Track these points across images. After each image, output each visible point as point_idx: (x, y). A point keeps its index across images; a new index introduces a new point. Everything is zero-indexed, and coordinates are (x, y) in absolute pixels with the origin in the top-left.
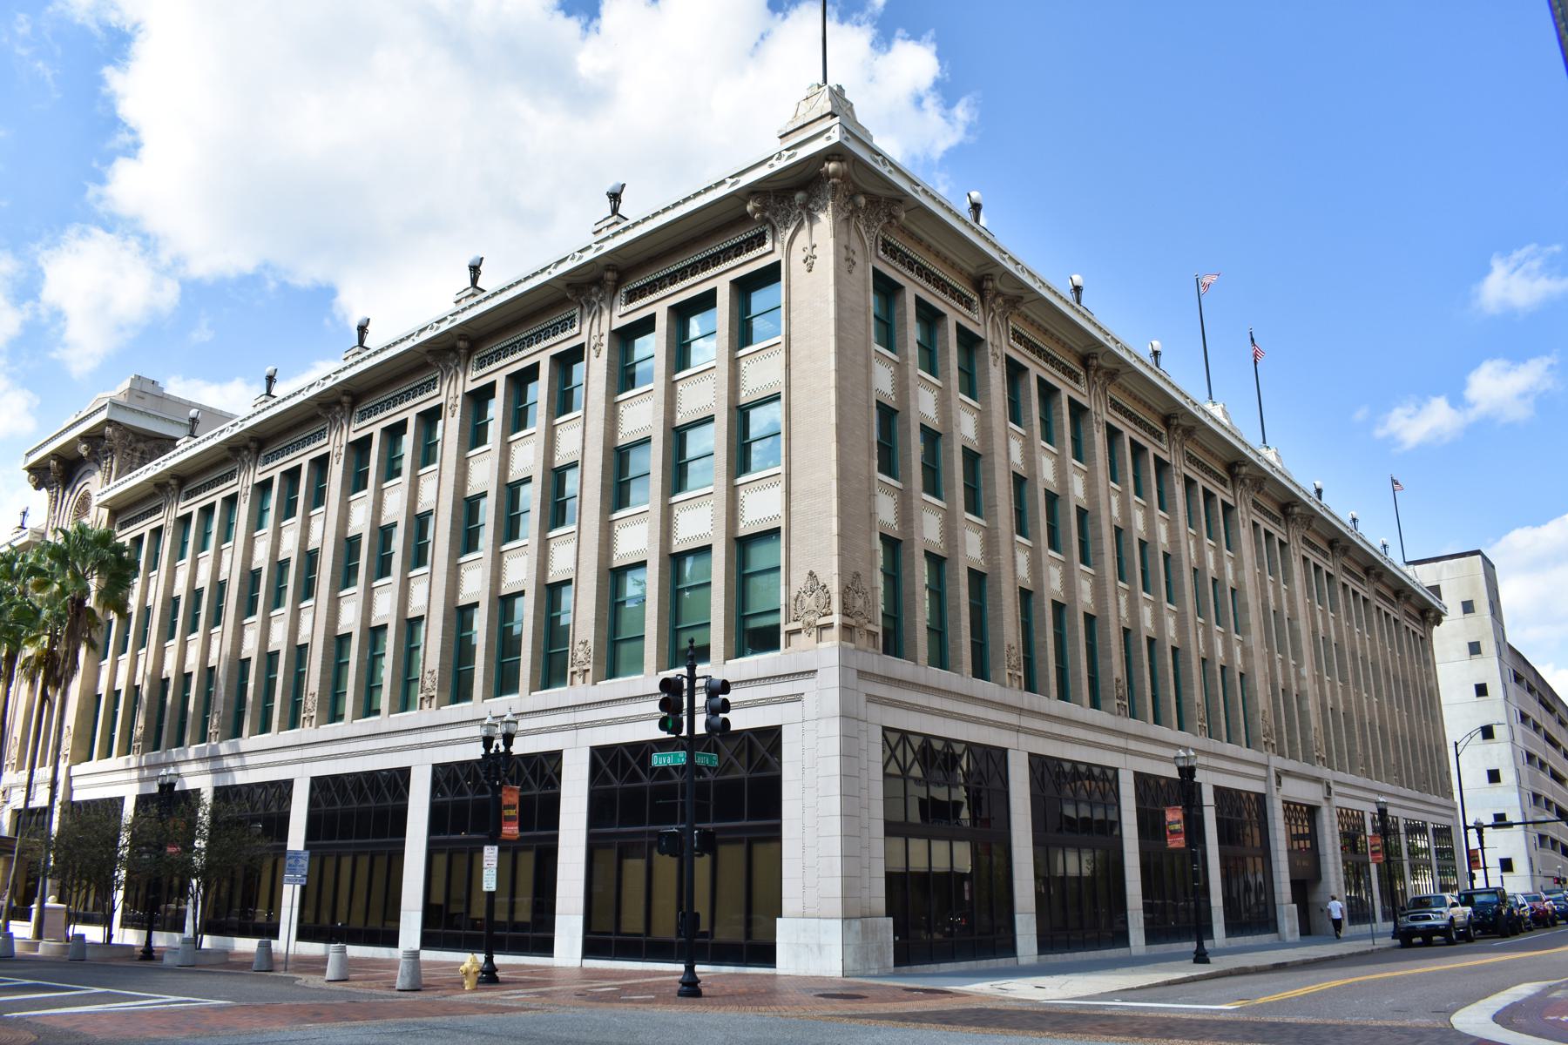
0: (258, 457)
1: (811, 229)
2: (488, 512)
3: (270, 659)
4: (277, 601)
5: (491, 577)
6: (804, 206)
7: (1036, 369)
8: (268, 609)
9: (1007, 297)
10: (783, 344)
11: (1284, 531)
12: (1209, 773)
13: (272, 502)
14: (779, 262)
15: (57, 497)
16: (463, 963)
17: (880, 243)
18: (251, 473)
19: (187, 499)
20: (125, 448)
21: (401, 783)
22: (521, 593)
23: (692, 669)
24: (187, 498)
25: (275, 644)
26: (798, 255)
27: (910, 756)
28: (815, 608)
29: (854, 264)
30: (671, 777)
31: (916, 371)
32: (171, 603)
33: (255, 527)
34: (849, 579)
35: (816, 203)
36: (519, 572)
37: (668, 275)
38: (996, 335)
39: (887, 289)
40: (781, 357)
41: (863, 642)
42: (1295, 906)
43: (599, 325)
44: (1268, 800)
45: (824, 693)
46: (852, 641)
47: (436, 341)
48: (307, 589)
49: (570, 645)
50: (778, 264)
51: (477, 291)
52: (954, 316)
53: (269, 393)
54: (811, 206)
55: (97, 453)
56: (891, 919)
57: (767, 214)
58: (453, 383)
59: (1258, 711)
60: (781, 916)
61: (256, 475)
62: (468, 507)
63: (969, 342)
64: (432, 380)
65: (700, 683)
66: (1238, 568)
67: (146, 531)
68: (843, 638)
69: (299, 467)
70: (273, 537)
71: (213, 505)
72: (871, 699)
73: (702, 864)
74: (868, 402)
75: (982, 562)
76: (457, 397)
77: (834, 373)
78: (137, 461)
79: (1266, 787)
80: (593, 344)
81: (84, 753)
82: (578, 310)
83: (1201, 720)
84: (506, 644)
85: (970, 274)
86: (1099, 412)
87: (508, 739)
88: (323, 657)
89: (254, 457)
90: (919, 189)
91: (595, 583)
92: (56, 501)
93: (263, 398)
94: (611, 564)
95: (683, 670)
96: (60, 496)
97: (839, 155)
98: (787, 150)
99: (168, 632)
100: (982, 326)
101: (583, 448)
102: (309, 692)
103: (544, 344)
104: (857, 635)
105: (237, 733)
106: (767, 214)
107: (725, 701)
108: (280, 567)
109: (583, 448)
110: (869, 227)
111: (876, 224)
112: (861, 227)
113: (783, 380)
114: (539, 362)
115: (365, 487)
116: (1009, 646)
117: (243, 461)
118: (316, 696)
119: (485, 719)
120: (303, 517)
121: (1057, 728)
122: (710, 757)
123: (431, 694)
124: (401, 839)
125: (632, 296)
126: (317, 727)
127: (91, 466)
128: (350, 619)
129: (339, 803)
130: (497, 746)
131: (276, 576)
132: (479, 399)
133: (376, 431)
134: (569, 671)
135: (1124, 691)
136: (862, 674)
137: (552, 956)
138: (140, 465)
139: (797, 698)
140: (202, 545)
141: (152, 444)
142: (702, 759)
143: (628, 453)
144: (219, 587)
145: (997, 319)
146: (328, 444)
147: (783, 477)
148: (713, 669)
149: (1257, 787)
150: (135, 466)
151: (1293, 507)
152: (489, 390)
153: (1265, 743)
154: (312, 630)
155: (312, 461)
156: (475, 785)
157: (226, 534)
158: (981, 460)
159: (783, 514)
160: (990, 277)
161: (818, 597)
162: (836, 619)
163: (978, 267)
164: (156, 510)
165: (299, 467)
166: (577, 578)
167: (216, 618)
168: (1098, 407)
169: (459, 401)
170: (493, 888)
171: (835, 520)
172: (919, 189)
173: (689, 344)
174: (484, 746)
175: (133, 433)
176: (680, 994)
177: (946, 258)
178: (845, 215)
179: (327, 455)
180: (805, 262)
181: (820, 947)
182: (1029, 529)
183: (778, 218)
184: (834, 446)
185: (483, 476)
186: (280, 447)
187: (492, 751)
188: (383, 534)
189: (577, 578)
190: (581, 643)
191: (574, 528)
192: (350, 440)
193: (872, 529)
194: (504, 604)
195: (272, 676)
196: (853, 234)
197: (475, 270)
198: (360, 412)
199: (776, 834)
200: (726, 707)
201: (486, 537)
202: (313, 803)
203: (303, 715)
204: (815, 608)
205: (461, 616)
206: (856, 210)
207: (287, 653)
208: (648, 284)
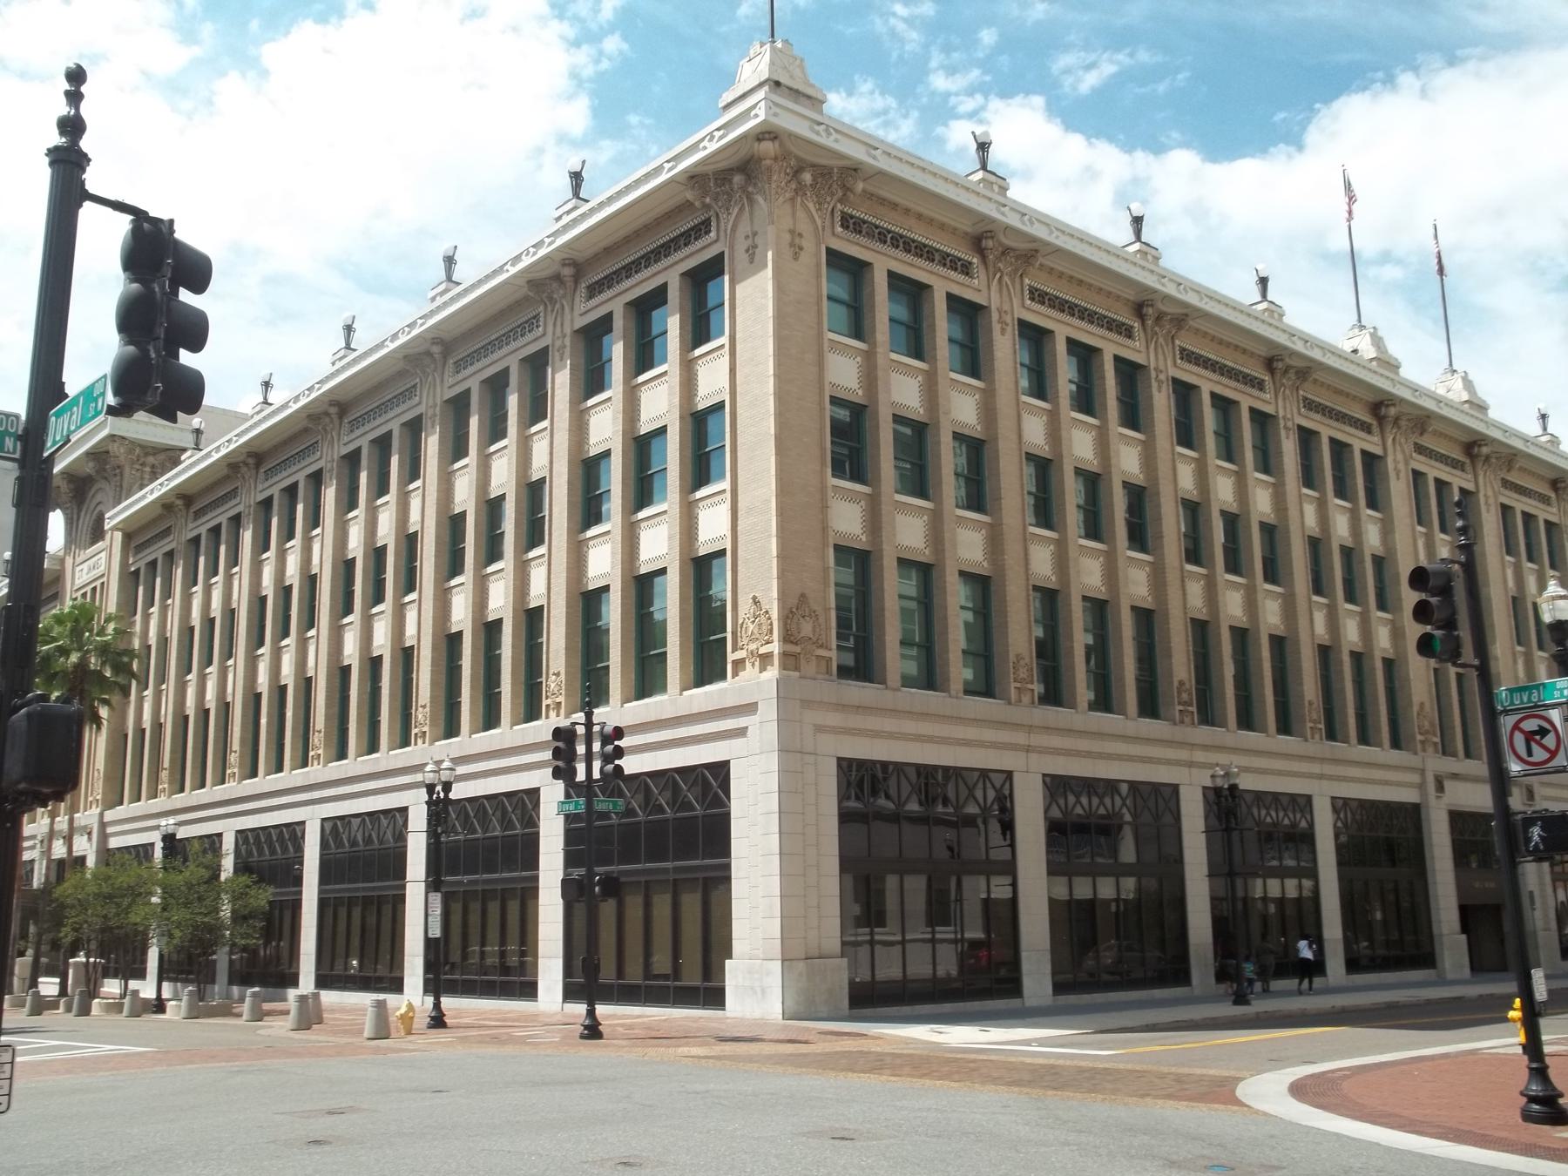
0: (257, 473)
1: (751, 214)
2: (615, 479)
3: (373, 664)
4: (492, 551)
5: (473, 602)
6: (743, 189)
7: (1063, 328)
8: (400, 594)
9: (1018, 253)
10: (727, 346)
11: (1470, 476)
12: (1325, 783)
13: (513, 401)
14: (723, 253)
15: (72, 519)
16: (399, 1009)
17: (838, 218)
18: (253, 493)
19: (195, 519)
20: (133, 463)
21: (530, 806)
22: (663, 571)
23: (589, 716)
24: (196, 518)
25: (649, 561)
26: (741, 245)
27: (906, 789)
28: (758, 636)
29: (801, 248)
30: (610, 819)
31: (1118, 430)
32: (454, 525)
33: (191, 584)
34: (793, 601)
35: (755, 184)
36: (603, 563)
37: (624, 268)
38: (1006, 298)
39: (851, 269)
40: (725, 361)
41: (810, 668)
42: (1464, 937)
43: (562, 325)
44: (1423, 811)
45: (764, 728)
46: (797, 669)
47: (713, 160)
48: (534, 533)
49: (544, 676)
50: (722, 254)
51: (452, 285)
52: (942, 283)
53: (449, 278)
54: (750, 189)
55: (105, 470)
56: (846, 960)
57: (708, 200)
58: (432, 390)
59: (1410, 704)
60: (731, 958)
61: (446, 389)
62: (589, 470)
63: (968, 313)
64: (534, 317)
65: (596, 728)
66: (1387, 530)
67: (300, 477)
68: (784, 666)
69: (389, 434)
70: (277, 561)
71: (389, 435)
72: (819, 729)
73: (608, 909)
74: (820, 404)
75: (985, 564)
76: (564, 336)
77: (772, 379)
78: (147, 476)
79: (1421, 795)
80: (429, 414)
81: (114, 799)
82: (541, 308)
83: (1314, 721)
84: (646, 632)
85: (966, 233)
86: (1162, 367)
87: (447, 787)
88: (327, 692)
89: (254, 472)
90: (878, 153)
91: (565, 609)
92: (72, 523)
93: (443, 287)
94: (404, 643)
95: (580, 717)
96: (75, 517)
97: (769, 133)
98: (668, 161)
99: (453, 564)
100: (985, 290)
101: (551, 462)
102: (551, 672)
103: (514, 345)
104: (803, 661)
105: (280, 769)
106: (708, 200)
107: (618, 747)
108: (377, 555)
109: (551, 462)
110: (820, 204)
111: (828, 199)
112: (811, 205)
113: (727, 386)
114: (469, 389)
115: (466, 454)
116: (1017, 656)
117: (244, 478)
118: (563, 677)
119: (426, 764)
120: (367, 509)
121: (1084, 744)
122: (615, 804)
123: (558, 700)
124: (725, 860)
125: (594, 290)
126: (324, 766)
127: (102, 484)
128: (461, 614)
129: (291, 849)
130: (438, 793)
131: (282, 603)
132: (459, 406)
133: (474, 385)
134: (731, 657)
135: (1190, 694)
136: (807, 704)
137: (724, 1010)
138: (152, 480)
139: (741, 732)
140: (381, 488)
141: (162, 457)
142: (602, 804)
143: (706, 418)
144: (410, 542)
145: (1006, 278)
146: (544, 335)
147: (728, 495)
148: (608, 715)
149: (1408, 796)
150: (146, 482)
151: (1480, 446)
152: (603, 326)
153: (1423, 742)
154: (419, 627)
155: (209, 530)
156: (705, 795)
157: (413, 470)
158: (987, 446)
159: (729, 535)
160: (990, 234)
161: (760, 625)
162: (775, 648)
163: (974, 225)
164: (167, 532)
165: (389, 434)
166: (549, 604)
167: (409, 582)
168: (1161, 357)
169: (568, 341)
170: (438, 935)
171: (774, 540)
172: (878, 153)
173: (652, 342)
174: (428, 793)
175: (140, 446)
176: (583, 1037)
177: (932, 220)
178: (788, 195)
179: (545, 351)
180: (747, 251)
181: (763, 991)
182: (1055, 519)
183: (720, 204)
184: (773, 459)
185: (605, 429)
186: (277, 462)
187: (435, 796)
188: (492, 508)
189: (549, 604)
190: (554, 674)
191: (725, 485)
192: (577, 326)
193: (825, 545)
194: (642, 586)
195: (645, 611)
196: (801, 214)
197: (349, 329)
198: (350, 422)
199: (533, 885)
200: (619, 752)
201: (614, 505)
202: (324, 844)
203: (414, 731)
204: (758, 636)
205: (589, 602)
206: (800, 189)
207: (295, 687)
208: (605, 278)
